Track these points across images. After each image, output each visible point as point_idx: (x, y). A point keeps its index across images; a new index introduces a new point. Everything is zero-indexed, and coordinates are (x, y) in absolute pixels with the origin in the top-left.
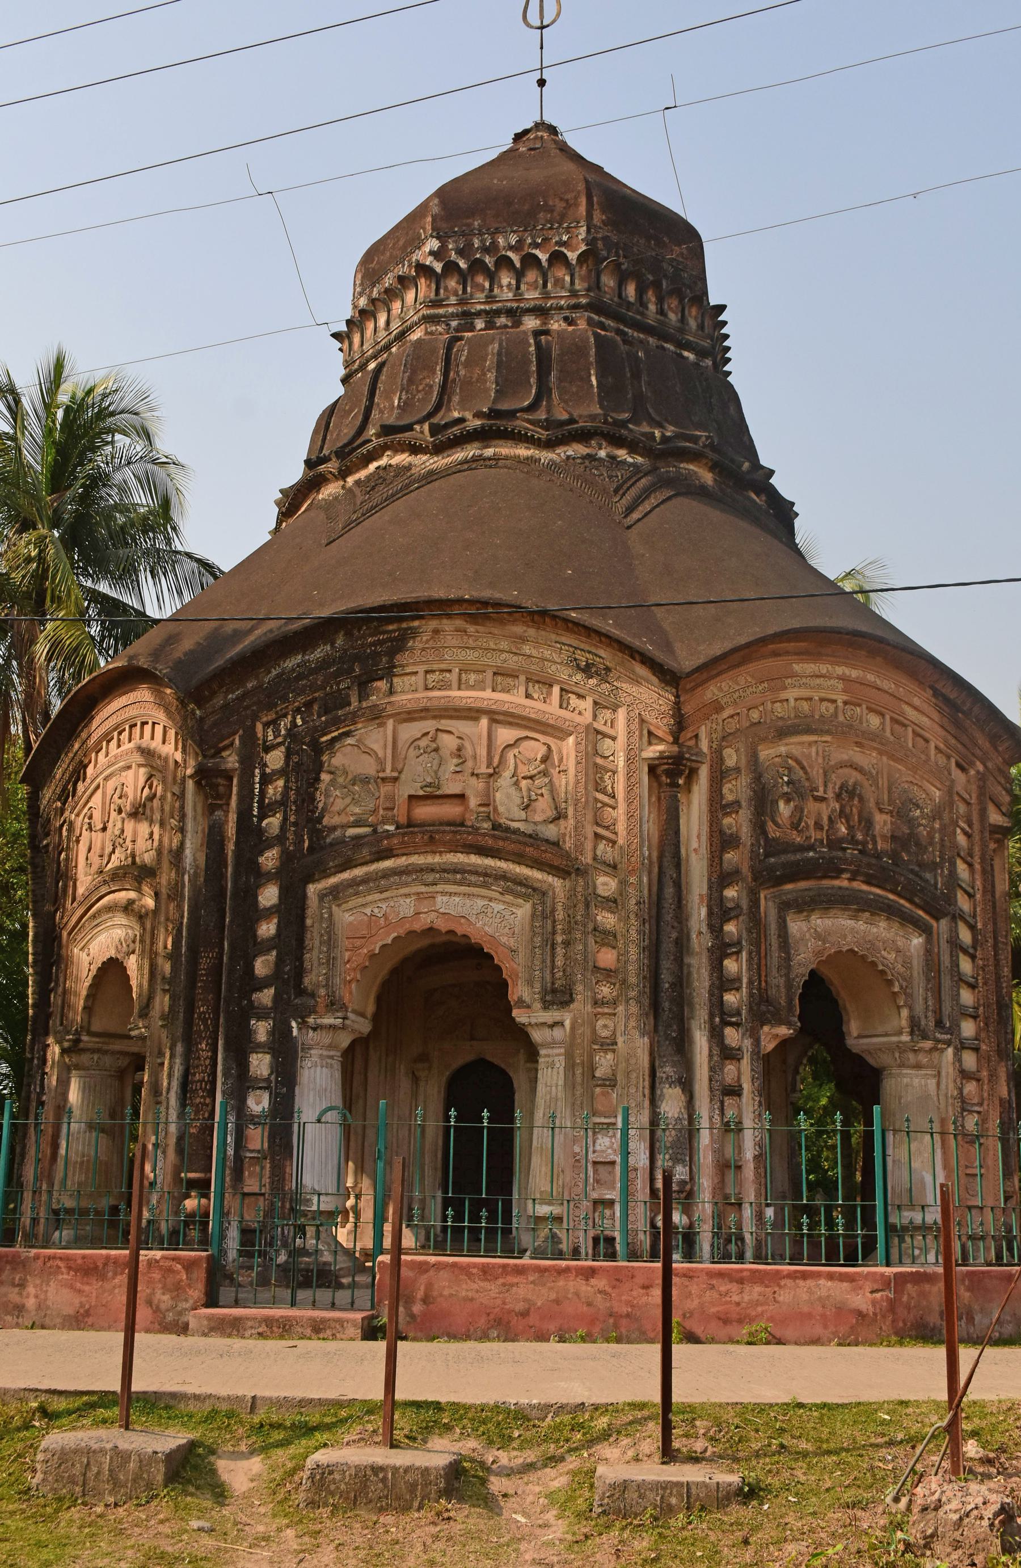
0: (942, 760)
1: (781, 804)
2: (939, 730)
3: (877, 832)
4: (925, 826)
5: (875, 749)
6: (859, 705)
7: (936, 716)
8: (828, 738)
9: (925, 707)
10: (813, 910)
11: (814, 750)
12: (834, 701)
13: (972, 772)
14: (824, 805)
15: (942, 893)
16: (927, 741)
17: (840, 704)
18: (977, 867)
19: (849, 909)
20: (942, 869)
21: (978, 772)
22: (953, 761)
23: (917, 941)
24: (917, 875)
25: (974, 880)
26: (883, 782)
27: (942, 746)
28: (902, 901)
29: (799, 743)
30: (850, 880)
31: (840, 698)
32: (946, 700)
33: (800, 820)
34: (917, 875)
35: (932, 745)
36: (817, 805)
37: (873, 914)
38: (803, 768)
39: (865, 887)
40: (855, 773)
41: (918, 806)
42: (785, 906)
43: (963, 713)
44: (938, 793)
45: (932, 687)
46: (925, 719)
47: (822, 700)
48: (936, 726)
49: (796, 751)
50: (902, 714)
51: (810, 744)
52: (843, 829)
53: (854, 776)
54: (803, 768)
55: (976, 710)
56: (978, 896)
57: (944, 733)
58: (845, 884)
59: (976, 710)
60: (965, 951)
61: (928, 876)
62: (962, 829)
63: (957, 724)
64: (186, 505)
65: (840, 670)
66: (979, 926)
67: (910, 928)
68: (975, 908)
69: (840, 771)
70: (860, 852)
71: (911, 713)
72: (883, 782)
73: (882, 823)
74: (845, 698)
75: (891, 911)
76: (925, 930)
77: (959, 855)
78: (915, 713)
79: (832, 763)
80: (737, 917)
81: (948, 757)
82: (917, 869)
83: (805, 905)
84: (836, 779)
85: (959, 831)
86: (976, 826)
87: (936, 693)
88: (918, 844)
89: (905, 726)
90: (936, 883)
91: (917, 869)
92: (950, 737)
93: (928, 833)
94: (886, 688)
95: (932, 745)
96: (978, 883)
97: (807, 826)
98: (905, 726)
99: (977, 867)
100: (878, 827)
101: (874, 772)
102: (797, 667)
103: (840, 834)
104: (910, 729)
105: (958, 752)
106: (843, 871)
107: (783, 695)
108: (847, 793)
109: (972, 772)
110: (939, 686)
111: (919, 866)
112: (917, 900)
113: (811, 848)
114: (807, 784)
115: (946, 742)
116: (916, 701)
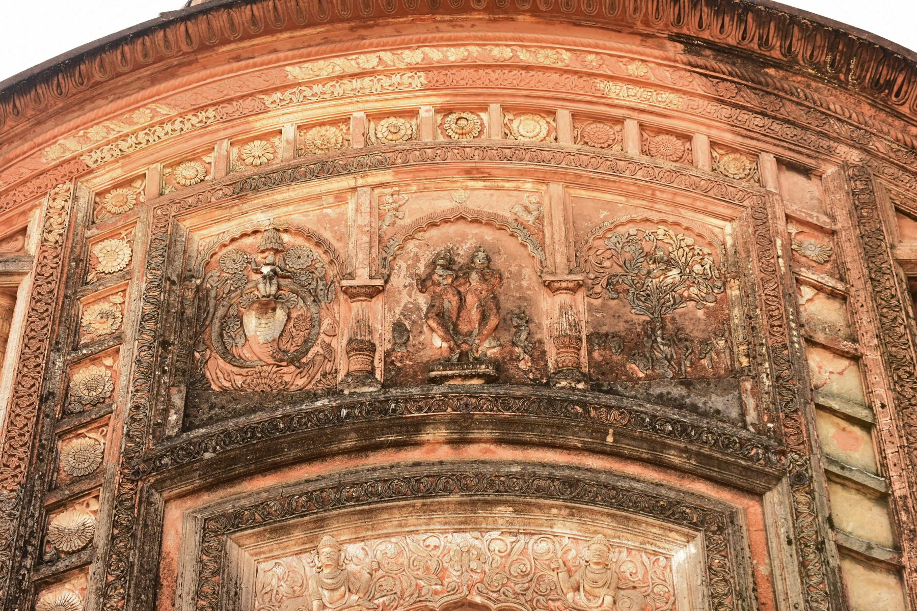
1: (251, 321)
3: (544, 335)
4: (699, 301)
5: (523, 173)
6: (484, 108)
7: (698, 84)
8: (387, 176)
9: (666, 76)
10: (320, 523)
11: (351, 206)
13: (830, 170)
16: (687, 137)
18: (873, 357)
19: (442, 508)
20: (756, 378)
21: (845, 166)
22: (768, 163)
23: (683, 555)
24: (679, 405)
25: (869, 391)
26: (555, 232)
27: (728, 137)
28: (633, 469)
30: (455, 443)
31: (426, 106)
32: (722, 51)
35: (701, 144)
37: (520, 509)
39: (506, 453)
41: (669, 263)
42: (220, 527)
43: (777, 65)
44: (728, 227)
45: (676, 38)
46: (666, 96)
47: (376, 116)
49: (298, 216)
51: (340, 197)
52: (438, 342)
55: (799, 47)
56: (885, 422)
57: (726, 111)
58: (445, 453)
59: (799, 47)
60: (867, 560)
62: (819, 288)
64: (831, 301)
65: (413, 56)
66: (899, 489)
67: (652, 526)
68: (882, 451)
69: (434, 232)
71: (618, 92)
72: (555, 232)
75: (574, 492)
76: (713, 526)
77: (811, 342)
78: (635, 90)
80: (82, 567)
82: (677, 391)
83: (274, 519)
86: (856, 270)
87: (691, 44)
91: (677, 391)
92: (744, 116)
93: (710, 313)
94: (547, 63)
96: (882, 392)
98: (620, 121)
99: (873, 357)
100: (546, 322)
101: (530, 219)
102: (294, 72)
103: (426, 355)
104: (631, 127)
105: (779, 140)
106: (418, 425)
107: (262, 124)
109: (830, 170)
110: (690, 28)
111: (687, 383)
112: (674, 458)
115: (733, 126)
116: (635, 69)
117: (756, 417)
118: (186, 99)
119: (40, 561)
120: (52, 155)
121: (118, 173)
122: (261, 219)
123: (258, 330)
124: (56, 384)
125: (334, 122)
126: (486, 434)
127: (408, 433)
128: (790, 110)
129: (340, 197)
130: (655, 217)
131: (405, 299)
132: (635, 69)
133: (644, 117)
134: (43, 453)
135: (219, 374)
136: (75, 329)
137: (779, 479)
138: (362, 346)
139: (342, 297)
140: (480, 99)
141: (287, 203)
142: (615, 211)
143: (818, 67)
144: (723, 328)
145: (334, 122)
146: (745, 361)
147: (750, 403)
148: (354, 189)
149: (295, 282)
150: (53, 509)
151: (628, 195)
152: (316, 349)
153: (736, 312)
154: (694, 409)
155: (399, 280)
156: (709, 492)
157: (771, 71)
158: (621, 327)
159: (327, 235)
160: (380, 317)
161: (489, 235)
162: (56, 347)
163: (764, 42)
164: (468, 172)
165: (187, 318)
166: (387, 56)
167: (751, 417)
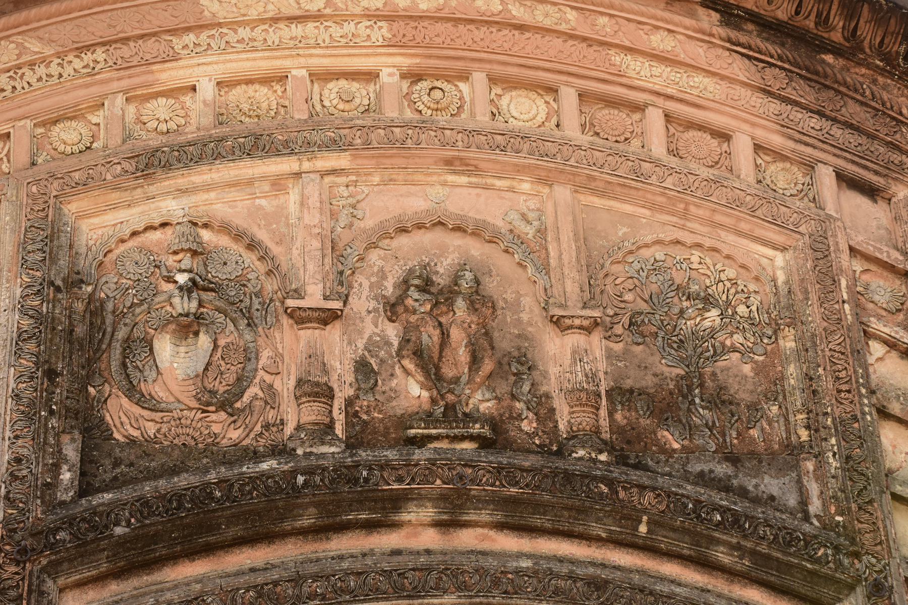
0: (783, 177)
1: (165, 348)
2: (758, 100)
3: (551, 386)
5: (520, 169)
6: (464, 76)
7: (739, 68)
8: (342, 161)
9: (699, 53)
11: (293, 197)
12: (371, 76)
14: (334, 332)
15: (828, 526)
16: (724, 136)
17: (389, 77)
20: (819, 456)
22: (826, 177)
24: (724, 486)
26: (563, 251)
27: (777, 140)
28: (670, 569)
29: (234, 184)
33: (241, 383)
34: (724, 486)
35: (742, 146)
36: (309, 335)
38: (252, 246)
39: (508, 542)
40: (456, 241)
41: (708, 301)
43: (837, 51)
44: (780, 259)
46: (699, 80)
48: (745, 93)
50: (618, 77)
51: (278, 184)
53: (447, 254)
54: (252, 246)
57: (775, 106)
58: (430, 539)
61: (771, 485)
62: (891, 344)
63: (816, 78)
69: (403, 241)
70: (485, 443)
71: (639, 70)
72: (563, 251)
73: (567, 360)
74: (406, 62)
77: (884, 413)
79: (369, 223)
81: (810, 166)
82: (722, 469)
84: (385, 268)
85: (877, 349)
88: (720, 400)
89: (638, 108)
90: (804, 503)
91: (722, 469)
92: (798, 115)
93: (759, 370)
94: (548, 23)
95: (742, 146)
97: (271, 396)
98: (638, 108)
100: (553, 371)
101: (529, 231)
103: (401, 406)
105: (841, 150)
106: (398, 501)
108: (428, 290)
111: (734, 459)
112: (723, 556)
113: (280, 451)
114: (270, 286)
115: (784, 126)
116: (660, 41)
125: (266, 81)
126: (485, 516)
127: (384, 511)
128: (853, 111)
129: (278, 184)
130: (689, 239)
131: (369, 329)
133: (672, 106)
137: (852, 588)
139: (285, 321)
140: (459, 65)
141: (208, 188)
142: (638, 227)
143: (888, 58)
144: (775, 390)
145: (266, 81)
146: (804, 435)
147: (813, 488)
148: (298, 175)
151: (653, 207)
152: (254, 390)
153: (792, 369)
154: (743, 493)
157: (829, 58)
158: (649, 381)
159: (262, 235)
161: (476, 249)
163: (823, 21)
164: (449, 162)
167: (815, 507)
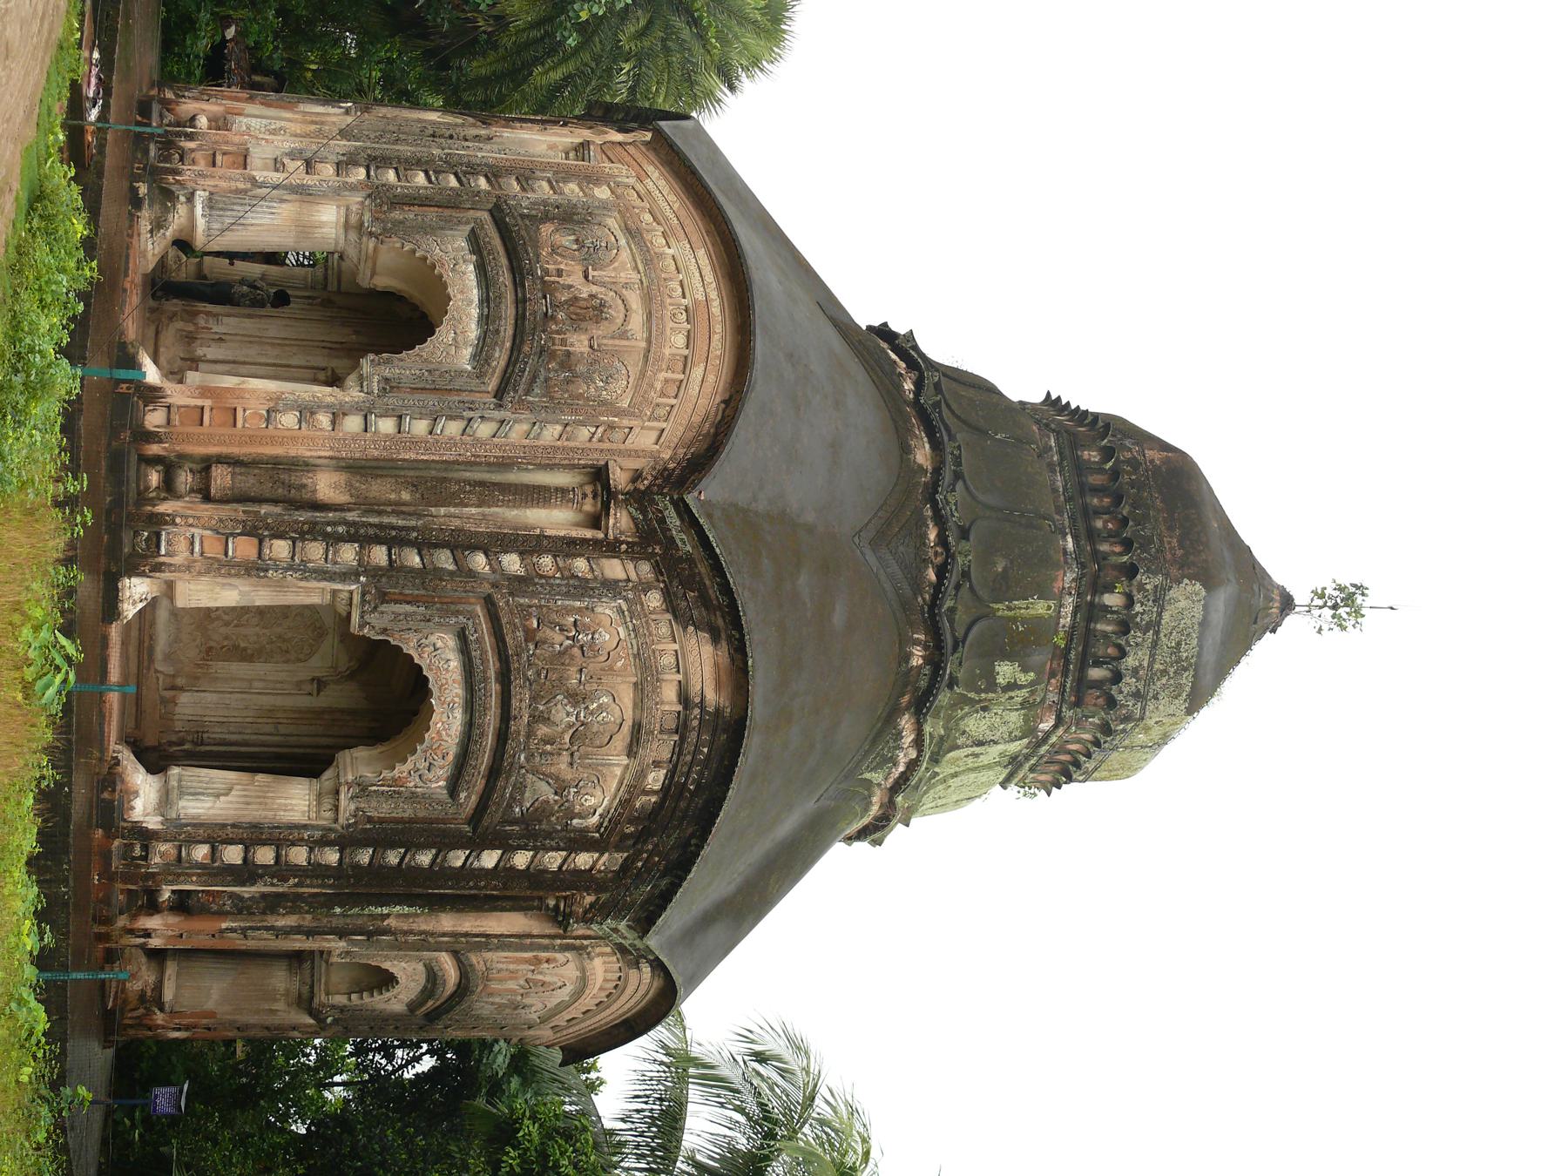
65: (713, 295)
102: (701, 253)
104: (681, 376)
111: (547, 380)
117: (619, 917)
118: (683, 213)
119: (465, 173)
120: (650, 169)
121: (642, 192)
122: (623, 242)
123: (567, 240)
124: (538, 174)
132: (711, 378)
134: (509, 171)
135: (546, 229)
136: (565, 181)
138: (559, 273)
149: (591, 257)
150: (486, 177)
155: (594, 289)
156: (515, 512)
160: (575, 279)
162: (556, 173)
165: (569, 216)
166: (656, 174)
